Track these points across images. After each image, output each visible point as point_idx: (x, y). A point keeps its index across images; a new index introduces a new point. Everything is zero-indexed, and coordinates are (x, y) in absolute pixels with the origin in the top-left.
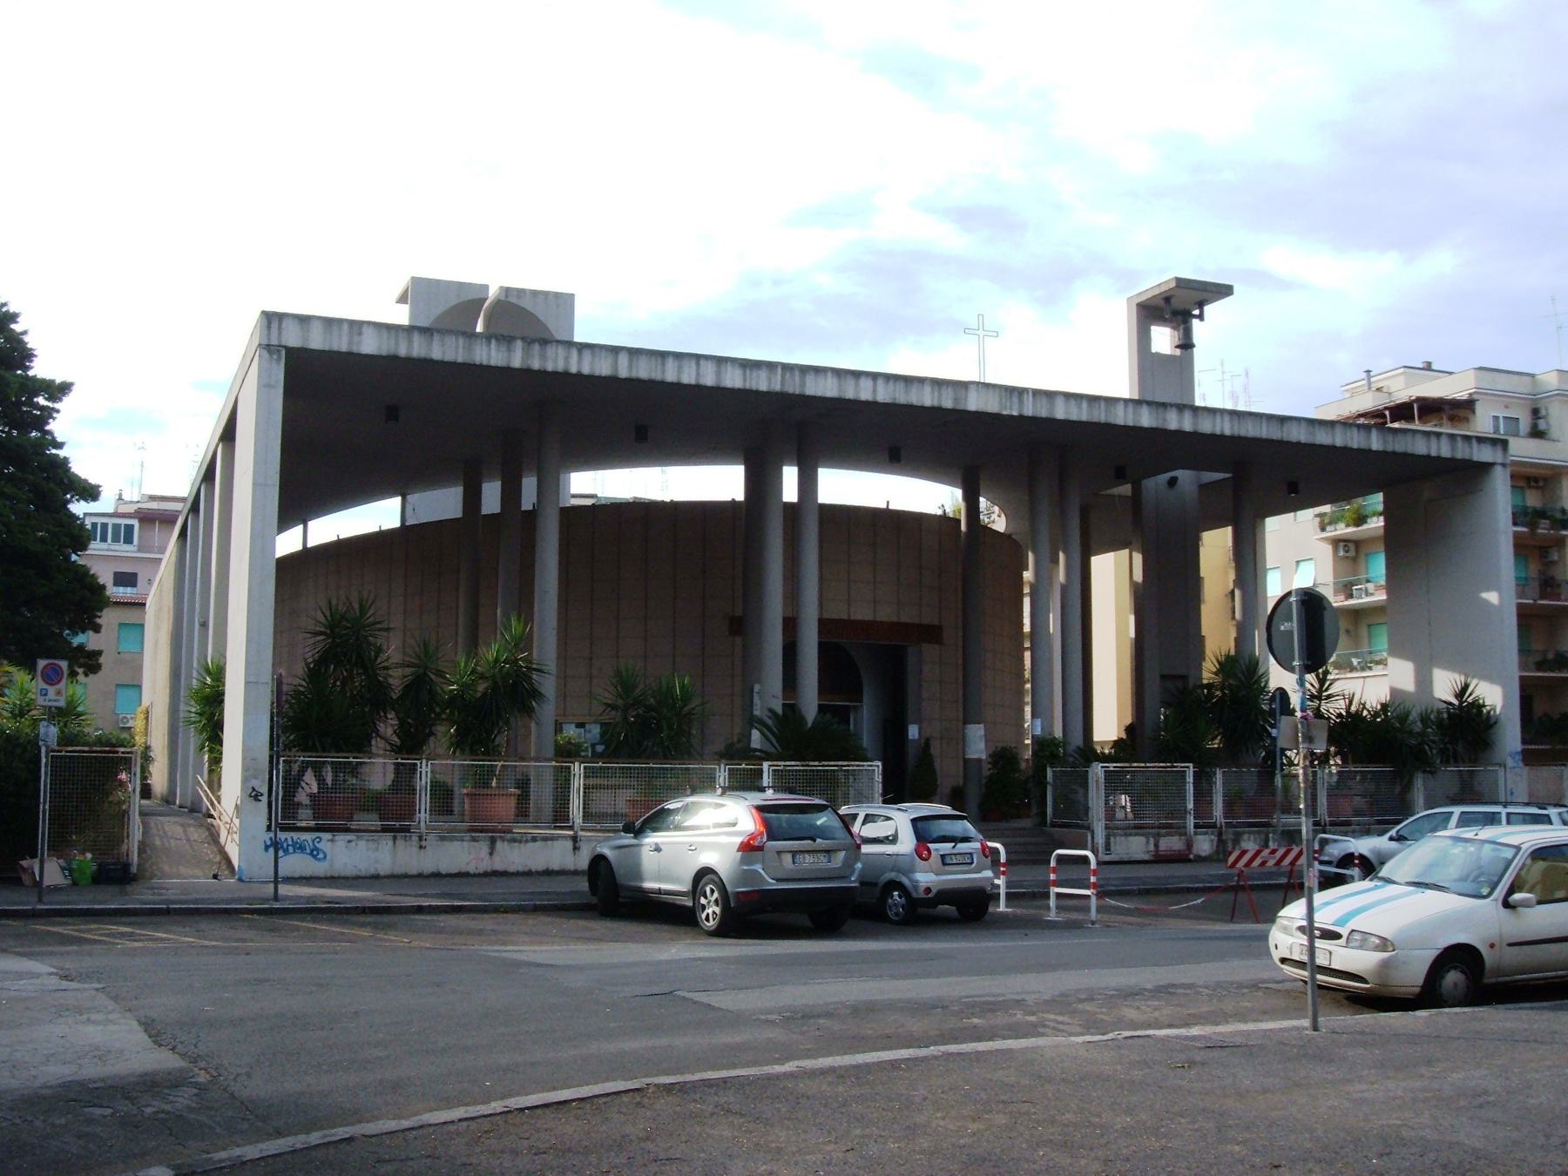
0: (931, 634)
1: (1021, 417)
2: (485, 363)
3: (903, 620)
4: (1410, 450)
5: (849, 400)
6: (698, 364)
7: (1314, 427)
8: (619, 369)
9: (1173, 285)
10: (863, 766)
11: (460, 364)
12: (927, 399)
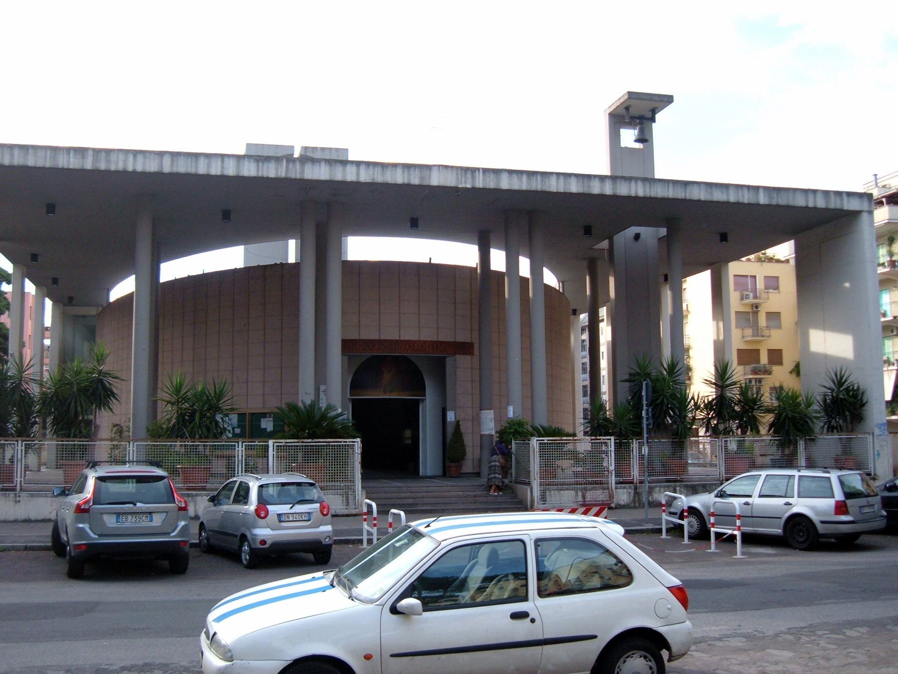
0: (465, 348)
1: (474, 189)
2: (65, 167)
3: (441, 339)
4: (791, 203)
5: (338, 182)
6: (223, 161)
7: (711, 188)
9: (626, 97)
10: (346, 442)
11: (48, 168)
12: (399, 178)
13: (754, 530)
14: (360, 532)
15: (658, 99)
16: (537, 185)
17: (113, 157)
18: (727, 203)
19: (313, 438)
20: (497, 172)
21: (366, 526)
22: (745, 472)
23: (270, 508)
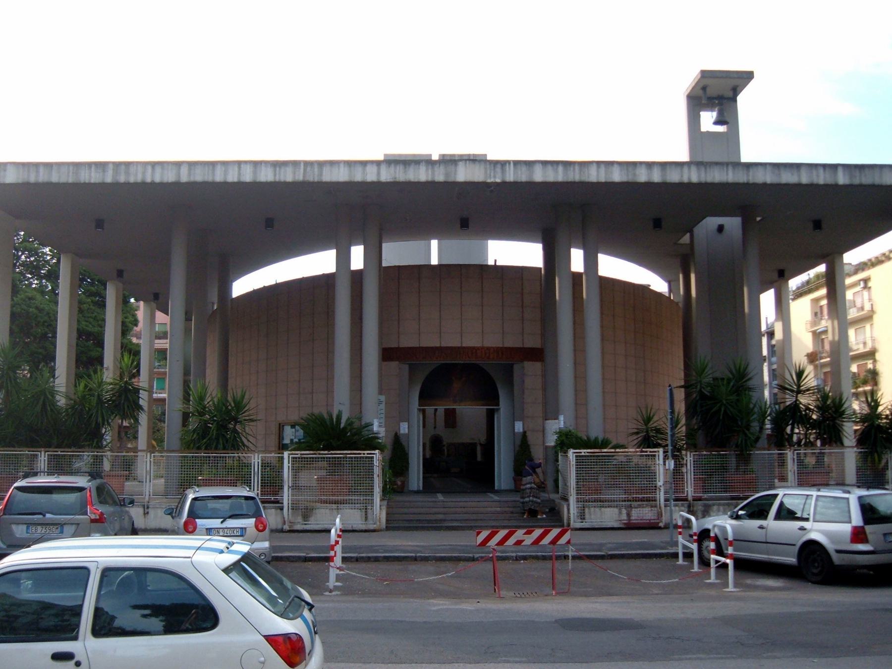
0: (535, 354)
1: (504, 183)
2: (87, 182)
3: (507, 345)
5: (358, 183)
6: (240, 168)
8: (181, 176)
11: (71, 184)
13: (769, 558)
14: (676, 544)
15: (736, 76)
16: (575, 176)
17: (132, 169)
18: (799, 185)
19: (329, 450)
20: (530, 164)
21: (680, 539)
22: (764, 491)
23: (199, 522)
